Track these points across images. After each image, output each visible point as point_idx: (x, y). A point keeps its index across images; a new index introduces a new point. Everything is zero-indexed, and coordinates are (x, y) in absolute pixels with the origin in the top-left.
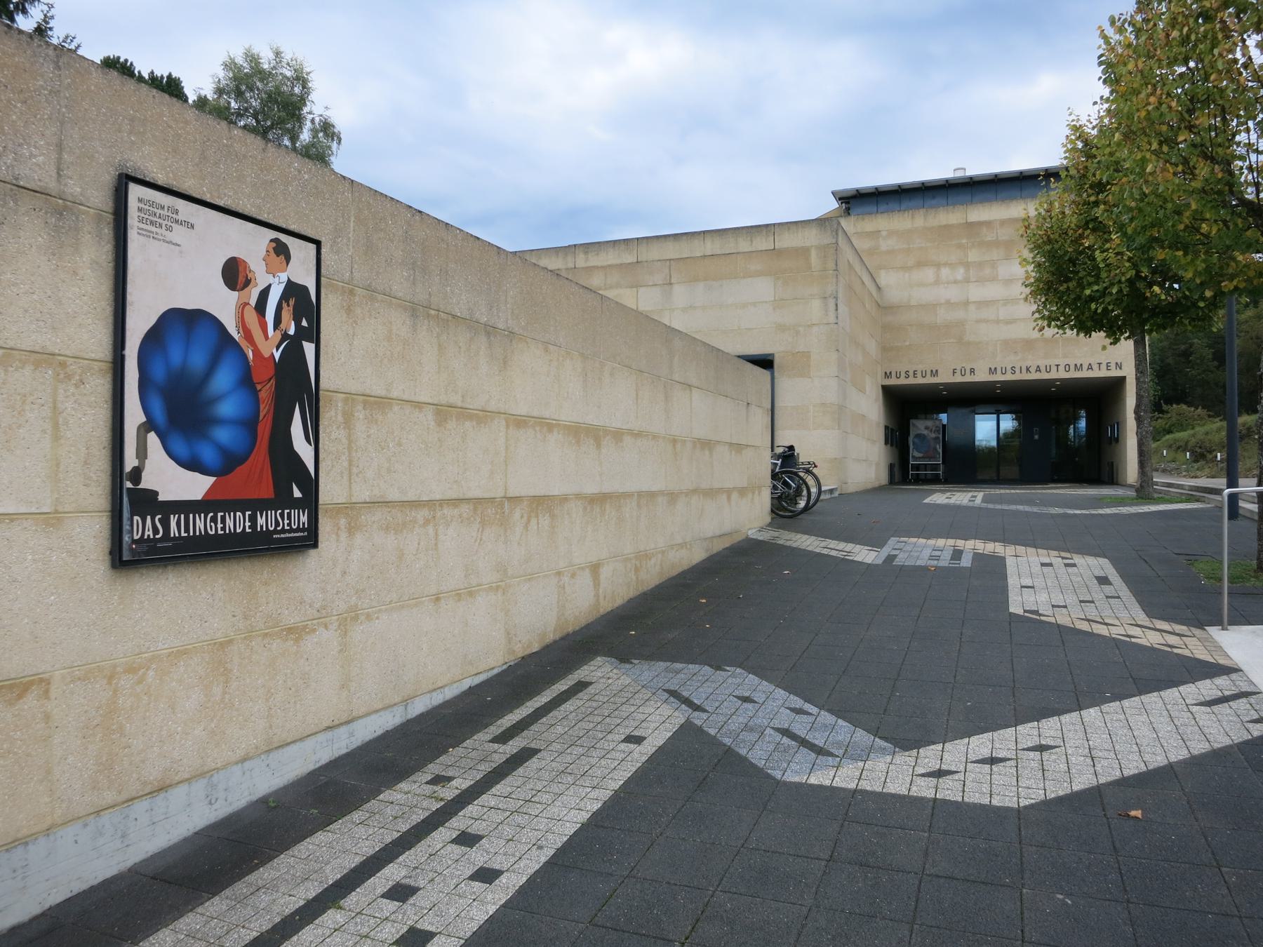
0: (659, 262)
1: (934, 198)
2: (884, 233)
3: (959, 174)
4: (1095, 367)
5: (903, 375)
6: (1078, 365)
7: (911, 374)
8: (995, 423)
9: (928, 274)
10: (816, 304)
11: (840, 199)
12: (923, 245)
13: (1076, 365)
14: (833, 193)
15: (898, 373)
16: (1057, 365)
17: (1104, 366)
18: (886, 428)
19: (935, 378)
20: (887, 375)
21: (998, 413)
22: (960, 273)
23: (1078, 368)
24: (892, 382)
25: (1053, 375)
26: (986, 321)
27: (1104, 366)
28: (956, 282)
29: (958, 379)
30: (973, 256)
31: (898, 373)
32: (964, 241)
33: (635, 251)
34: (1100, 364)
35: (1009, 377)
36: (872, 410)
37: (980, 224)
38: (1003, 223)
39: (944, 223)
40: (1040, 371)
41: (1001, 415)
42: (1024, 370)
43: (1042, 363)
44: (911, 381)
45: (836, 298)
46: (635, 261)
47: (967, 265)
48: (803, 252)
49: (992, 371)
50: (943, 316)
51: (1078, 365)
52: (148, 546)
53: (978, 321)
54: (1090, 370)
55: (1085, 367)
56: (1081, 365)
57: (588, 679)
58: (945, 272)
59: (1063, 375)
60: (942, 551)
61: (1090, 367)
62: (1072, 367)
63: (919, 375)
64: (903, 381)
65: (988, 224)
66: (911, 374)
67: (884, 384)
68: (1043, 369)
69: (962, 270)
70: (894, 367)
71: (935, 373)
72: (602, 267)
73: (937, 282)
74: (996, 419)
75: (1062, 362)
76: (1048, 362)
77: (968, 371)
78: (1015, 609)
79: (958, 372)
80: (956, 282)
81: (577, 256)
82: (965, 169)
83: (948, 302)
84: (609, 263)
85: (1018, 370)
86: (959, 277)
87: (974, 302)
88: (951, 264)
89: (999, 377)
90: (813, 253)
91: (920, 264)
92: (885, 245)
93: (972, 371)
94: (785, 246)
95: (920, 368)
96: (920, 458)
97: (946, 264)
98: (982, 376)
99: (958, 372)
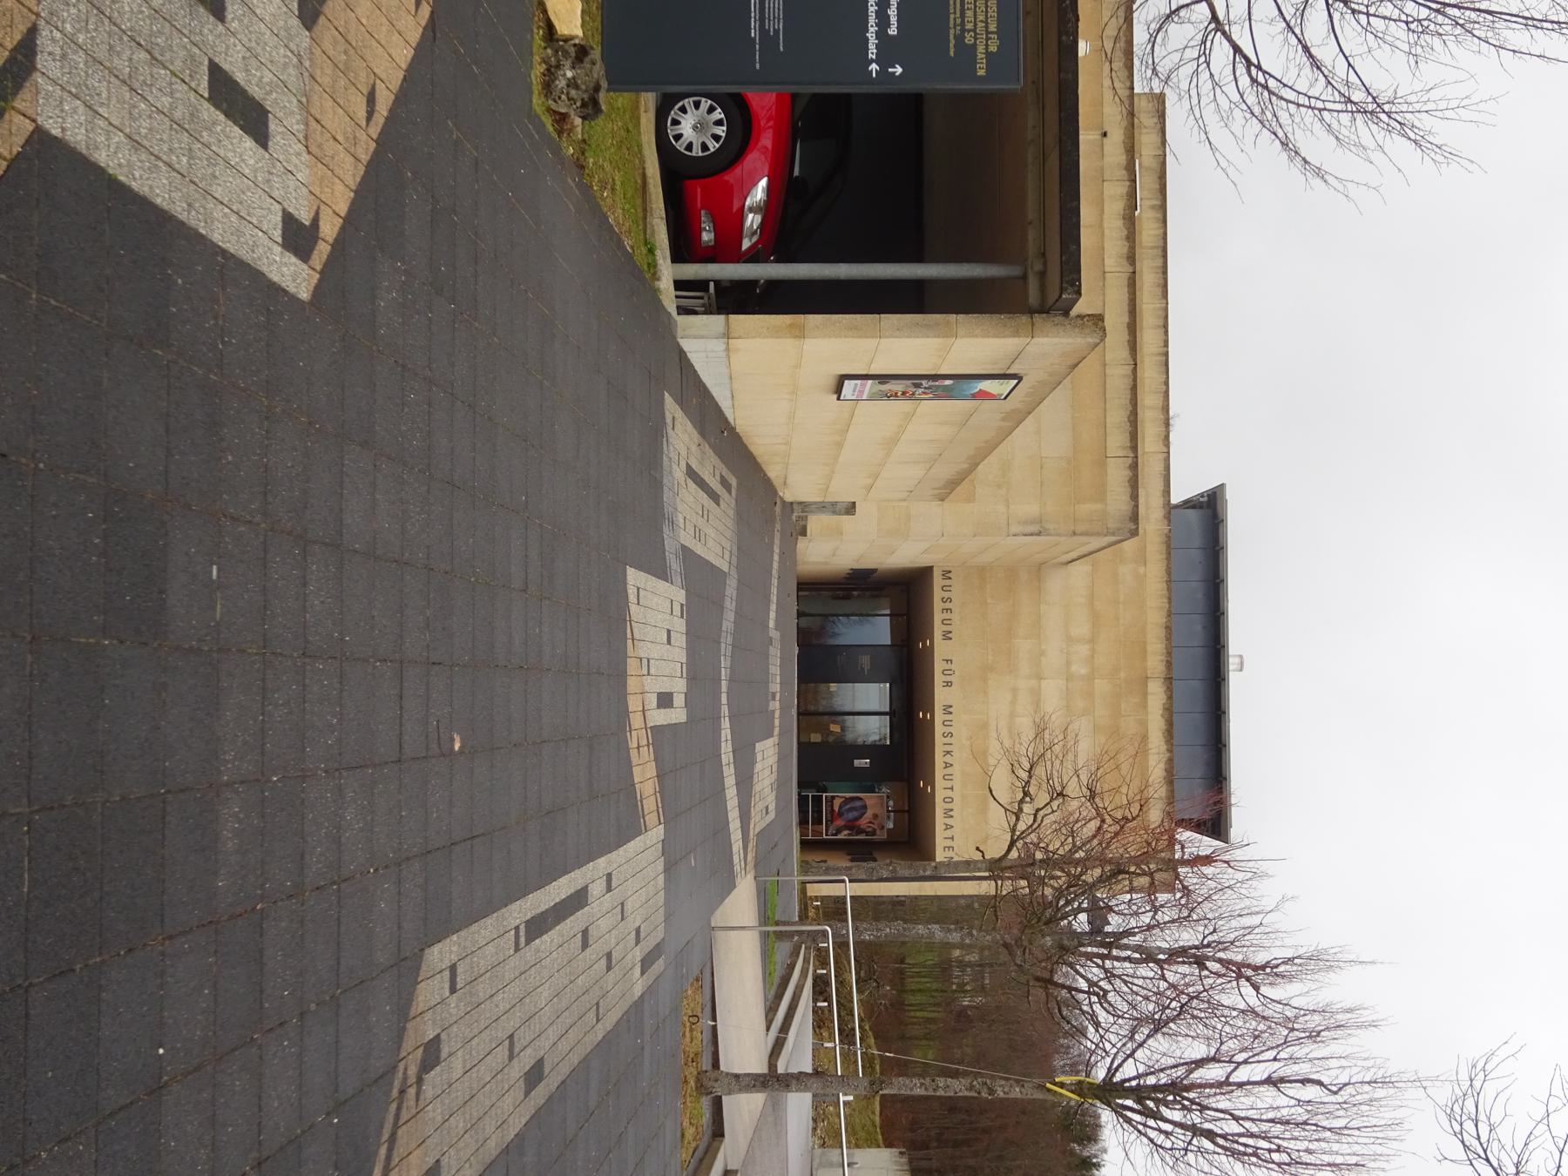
0: (1101, 304)
1: (1204, 627)
2: (1141, 570)
3: (1233, 663)
4: (949, 833)
5: (946, 595)
6: (949, 635)
7: (947, 605)
8: (875, 707)
9: (1081, 629)
10: (1030, 509)
11: (1215, 493)
12: (1121, 621)
13: (952, 810)
14: (1222, 486)
15: (949, 622)
16: (952, 788)
17: (949, 843)
18: (874, 571)
19: (941, 637)
20: (946, 574)
21: (891, 713)
22: (1080, 669)
23: (948, 813)
24: (938, 581)
25: (940, 783)
26: (1014, 702)
27: (949, 843)
28: (1068, 663)
29: (938, 667)
30: (1102, 686)
31: (949, 622)
32: (1123, 675)
33: (1118, 269)
34: (952, 838)
35: (939, 729)
36: (902, 555)
37: (1145, 695)
38: (1143, 724)
39: (1149, 648)
40: (946, 767)
41: (765, 1071)
42: (948, 748)
43: (956, 770)
44: (938, 605)
45: (1039, 534)
46: (1106, 270)
47: (1090, 678)
48: (1100, 494)
49: (948, 709)
50: (1023, 646)
51: (949, 635)
52: (777, 32)
53: (1014, 691)
54: (944, 827)
55: (949, 821)
56: (952, 817)
57: (722, 502)
58: (1083, 650)
59: (940, 795)
60: (638, 604)
61: (948, 827)
62: (949, 806)
63: (946, 616)
64: (938, 594)
65: (1144, 705)
66: (947, 605)
67: (935, 569)
68: (949, 771)
69: (1083, 671)
70: (957, 584)
71: (947, 636)
72: (1102, 220)
73: (1069, 639)
74: (882, 710)
75: (956, 794)
76: (957, 784)
77: (948, 678)
78: (759, 746)
79: (948, 666)
80: (1068, 663)
81: (1119, 183)
82: (1241, 670)
83: (1042, 653)
84: (1107, 232)
85: (947, 740)
86: (1074, 668)
87: (1040, 687)
88: (1093, 657)
89: (939, 717)
90: (1098, 506)
91: (1095, 618)
92: (1125, 570)
93: (948, 684)
94: (1109, 471)
95: (955, 617)
96: (832, 807)
97: (1093, 650)
98: (941, 696)
99: (948, 666)
